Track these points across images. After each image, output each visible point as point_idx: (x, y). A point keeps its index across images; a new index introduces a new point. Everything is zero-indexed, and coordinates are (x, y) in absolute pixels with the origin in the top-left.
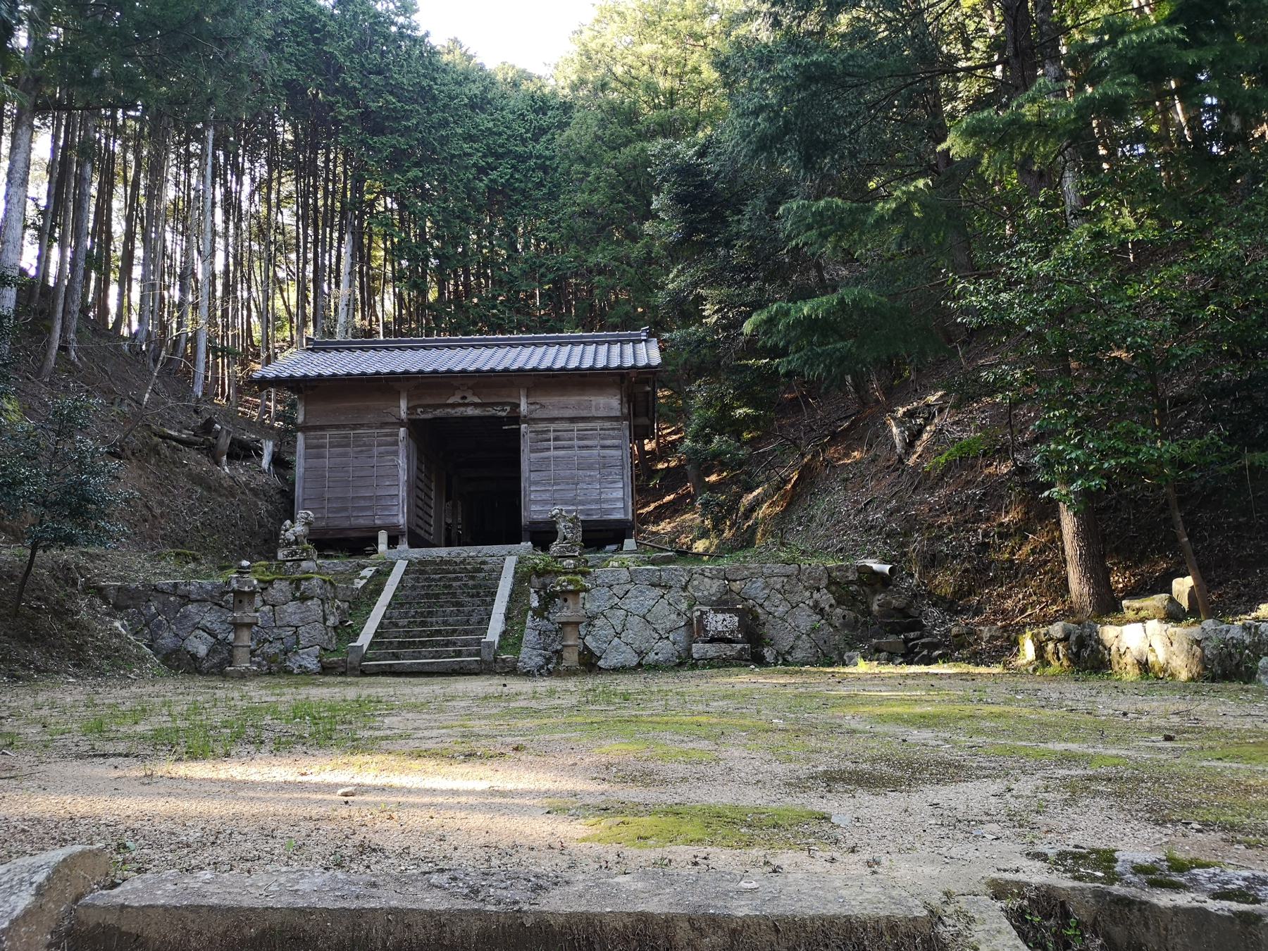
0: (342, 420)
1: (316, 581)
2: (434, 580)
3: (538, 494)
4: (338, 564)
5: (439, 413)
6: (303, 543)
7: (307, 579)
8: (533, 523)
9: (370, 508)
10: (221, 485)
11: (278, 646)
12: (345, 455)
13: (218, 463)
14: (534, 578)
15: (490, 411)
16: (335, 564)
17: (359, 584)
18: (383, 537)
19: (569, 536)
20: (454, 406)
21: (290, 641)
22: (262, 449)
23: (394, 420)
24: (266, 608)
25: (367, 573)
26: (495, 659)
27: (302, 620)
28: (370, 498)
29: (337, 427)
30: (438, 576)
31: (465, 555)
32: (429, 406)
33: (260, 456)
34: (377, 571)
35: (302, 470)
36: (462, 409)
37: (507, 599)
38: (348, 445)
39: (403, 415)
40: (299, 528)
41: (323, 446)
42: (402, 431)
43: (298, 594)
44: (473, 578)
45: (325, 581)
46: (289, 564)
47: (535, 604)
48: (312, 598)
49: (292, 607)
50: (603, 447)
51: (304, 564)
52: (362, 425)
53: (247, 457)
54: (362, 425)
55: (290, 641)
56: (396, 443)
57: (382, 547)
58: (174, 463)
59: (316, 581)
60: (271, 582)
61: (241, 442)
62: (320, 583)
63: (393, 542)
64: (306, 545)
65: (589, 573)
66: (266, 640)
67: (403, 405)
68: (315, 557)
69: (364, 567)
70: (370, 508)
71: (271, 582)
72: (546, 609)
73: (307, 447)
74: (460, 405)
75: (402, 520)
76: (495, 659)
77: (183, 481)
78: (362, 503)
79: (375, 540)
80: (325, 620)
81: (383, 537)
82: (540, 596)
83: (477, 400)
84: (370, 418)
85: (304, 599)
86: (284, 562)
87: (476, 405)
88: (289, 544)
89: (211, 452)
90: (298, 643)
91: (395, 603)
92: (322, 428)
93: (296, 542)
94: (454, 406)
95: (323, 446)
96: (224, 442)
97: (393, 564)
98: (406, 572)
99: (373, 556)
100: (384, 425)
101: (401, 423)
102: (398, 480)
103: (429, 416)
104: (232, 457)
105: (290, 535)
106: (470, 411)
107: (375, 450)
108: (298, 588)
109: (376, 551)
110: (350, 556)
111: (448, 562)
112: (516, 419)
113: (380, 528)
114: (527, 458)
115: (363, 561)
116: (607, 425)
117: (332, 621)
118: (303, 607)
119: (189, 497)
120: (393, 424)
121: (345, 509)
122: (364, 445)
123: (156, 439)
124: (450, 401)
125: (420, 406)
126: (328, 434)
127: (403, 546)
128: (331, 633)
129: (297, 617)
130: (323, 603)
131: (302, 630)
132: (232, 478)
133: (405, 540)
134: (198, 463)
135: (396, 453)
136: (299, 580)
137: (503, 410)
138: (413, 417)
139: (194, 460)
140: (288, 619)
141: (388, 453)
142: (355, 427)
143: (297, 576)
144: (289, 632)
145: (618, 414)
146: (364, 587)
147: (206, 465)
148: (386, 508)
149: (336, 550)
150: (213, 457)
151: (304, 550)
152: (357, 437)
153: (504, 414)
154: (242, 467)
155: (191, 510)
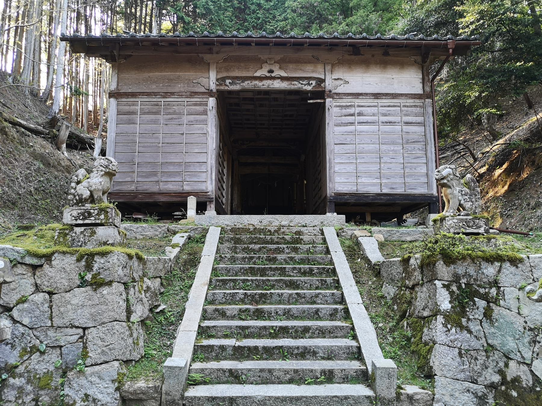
0: (154, 88)
1: (118, 256)
2: (253, 250)
3: (343, 166)
4: (147, 228)
5: (247, 85)
6: (100, 200)
7: (103, 254)
8: (339, 195)
9: (179, 173)
10: (59, 164)
11: (53, 359)
12: (155, 122)
13: (59, 149)
14: (440, 265)
15: (296, 85)
16: (144, 229)
17: (172, 253)
18: (192, 202)
19: (468, 205)
20: (261, 79)
21: (72, 352)
22: (94, 144)
23: (203, 90)
24: (40, 297)
25: (179, 239)
26: (399, 395)
27: (93, 317)
28: (180, 164)
29: (148, 94)
30: (257, 247)
31: (277, 223)
32: (237, 78)
33: (93, 149)
34: (189, 238)
35: (114, 135)
36: (269, 82)
37: (351, 275)
38: (157, 113)
39: (213, 87)
40: (97, 181)
41: (134, 113)
42: (212, 102)
43: (89, 277)
44: (296, 250)
45: (130, 257)
46: (78, 230)
47: (445, 305)
48: (110, 283)
49: (80, 295)
50: (407, 123)
51: (100, 230)
52: (173, 94)
53: (84, 149)
54: (173, 94)
55: (72, 352)
56: (205, 113)
57: (191, 211)
58: (21, 143)
59: (118, 256)
60: (48, 257)
61: (78, 137)
62: (124, 259)
63: (201, 208)
64: (106, 203)
65: (521, 261)
66: (34, 349)
67: (213, 76)
68: (117, 221)
69: (175, 233)
70: (179, 173)
71: (48, 257)
72: (463, 313)
73: (119, 113)
74: (267, 78)
75: (210, 186)
76: (399, 395)
77: (26, 157)
78: (171, 169)
79: (184, 205)
80: (129, 312)
81: (192, 202)
82: (452, 293)
83: (283, 74)
84: (179, 87)
85: (97, 284)
86: (72, 227)
87: (283, 79)
88: (81, 201)
89: (54, 140)
90: (85, 355)
91: (217, 281)
92: (133, 95)
93: (92, 199)
94: (261, 79)
95: (134, 113)
96: (64, 134)
97: (206, 231)
98: (221, 241)
99: (182, 221)
100: (193, 94)
101: (210, 93)
102: (207, 148)
103: (236, 87)
104: (70, 147)
105: (83, 191)
106: (277, 85)
107: (186, 119)
108: (89, 267)
109: (184, 216)
110: (158, 220)
111: (261, 231)
112: (321, 94)
113: (189, 194)
114: (333, 133)
115: (173, 226)
116: (410, 102)
117: (140, 312)
118: (96, 297)
119: (28, 168)
120: (203, 93)
121: (155, 174)
122: (174, 113)
123: (6, 124)
124: (258, 74)
125: (228, 78)
126: (139, 100)
127: (211, 212)
128: (139, 332)
129: (87, 312)
130: (127, 288)
131: (92, 334)
132: (70, 160)
133: (213, 206)
134: (42, 146)
135: (205, 122)
136: (92, 255)
137: (309, 84)
138: (222, 88)
139: (40, 145)
140: (71, 315)
141: (198, 122)
142: (166, 95)
143: (90, 248)
144: (73, 335)
145: (421, 92)
146: (177, 257)
147: (48, 148)
148: (195, 174)
149: (145, 214)
150: (56, 145)
151: (102, 210)
152: (168, 104)
153: (309, 88)
154: (79, 155)
155: (27, 178)
